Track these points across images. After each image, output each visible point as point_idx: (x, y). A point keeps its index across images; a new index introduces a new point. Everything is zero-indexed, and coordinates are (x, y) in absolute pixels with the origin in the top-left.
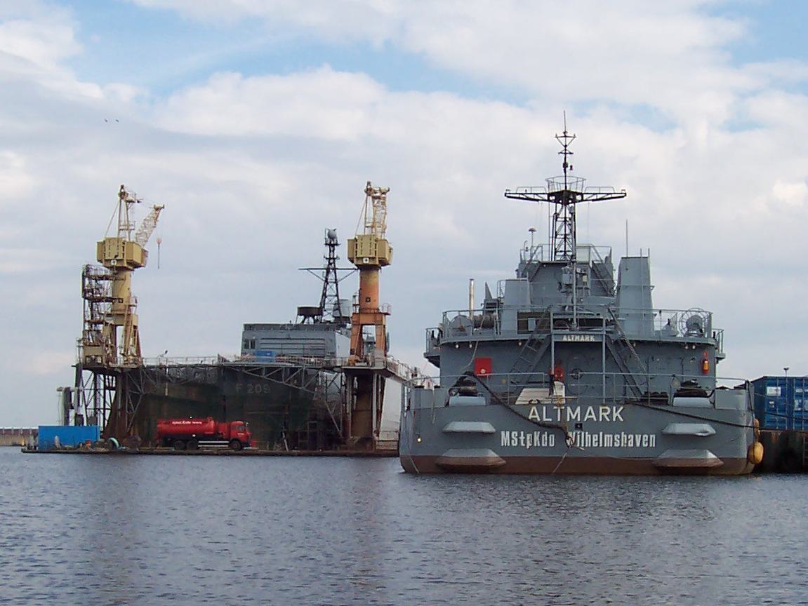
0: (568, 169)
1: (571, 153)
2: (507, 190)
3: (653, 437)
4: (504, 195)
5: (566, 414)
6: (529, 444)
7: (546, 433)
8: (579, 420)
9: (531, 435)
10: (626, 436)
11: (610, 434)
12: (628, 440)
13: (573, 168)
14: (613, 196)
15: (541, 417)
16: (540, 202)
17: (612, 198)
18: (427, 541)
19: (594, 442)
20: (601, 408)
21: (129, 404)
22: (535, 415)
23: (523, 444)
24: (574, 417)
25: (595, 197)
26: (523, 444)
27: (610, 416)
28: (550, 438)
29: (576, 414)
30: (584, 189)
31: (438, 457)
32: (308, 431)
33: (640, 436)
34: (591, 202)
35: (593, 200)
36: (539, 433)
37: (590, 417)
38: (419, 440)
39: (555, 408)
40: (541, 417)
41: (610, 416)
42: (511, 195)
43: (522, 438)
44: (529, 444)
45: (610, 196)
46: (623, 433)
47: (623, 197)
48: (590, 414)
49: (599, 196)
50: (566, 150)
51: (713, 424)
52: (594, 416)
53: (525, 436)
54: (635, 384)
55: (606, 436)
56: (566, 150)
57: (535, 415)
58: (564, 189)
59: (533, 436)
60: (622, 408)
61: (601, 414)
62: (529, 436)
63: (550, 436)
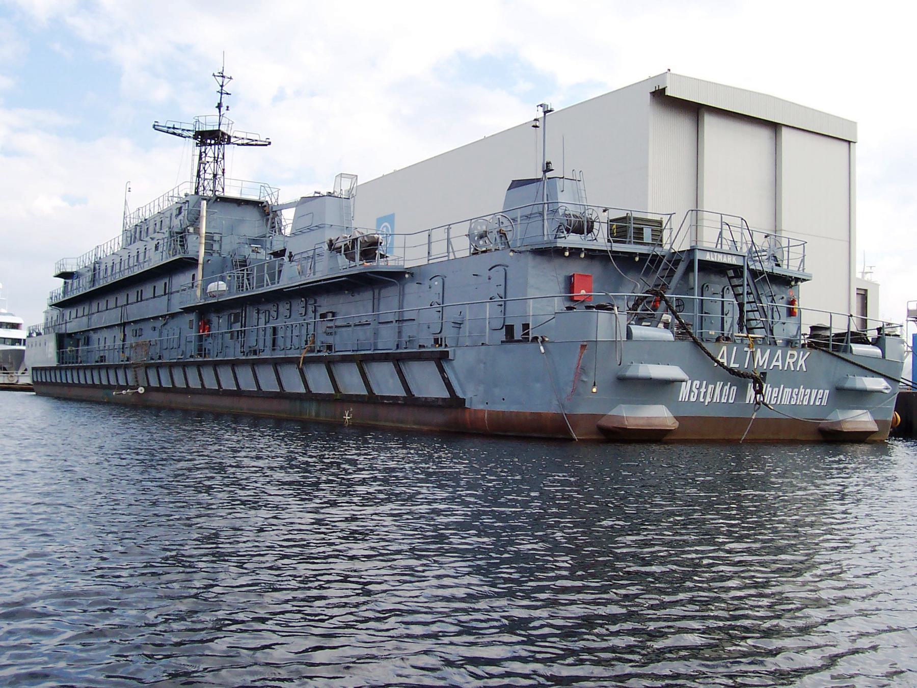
0: (223, 109)
1: (227, 94)
2: (156, 122)
3: (827, 392)
4: (152, 126)
5: (776, 354)
6: (708, 399)
7: (729, 384)
8: (765, 368)
9: (713, 386)
10: (803, 390)
11: (789, 388)
12: (805, 395)
13: (229, 109)
14: (259, 143)
15: (729, 361)
16: (187, 138)
17: (256, 145)
18: (162, 465)
19: (773, 397)
20: (790, 352)
21: (267, 281)
22: (723, 358)
23: (702, 400)
24: (761, 364)
25: (240, 142)
26: (702, 400)
27: (795, 363)
28: (732, 390)
29: (764, 359)
30: (232, 131)
31: (603, 416)
32: (80, 348)
33: (816, 390)
34: (236, 145)
35: (238, 145)
36: (722, 383)
37: (777, 364)
38: (594, 390)
39: (746, 349)
40: (729, 361)
41: (795, 363)
42: (161, 128)
43: (703, 390)
44: (708, 399)
45: (254, 143)
46: (802, 387)
47: (266, 145)
48: (777, 360)
49: (245, 141)
50: (222, 90)
51: (889, 381)
52: (780, 364)
53: (707, 387)
54: (766, 317)
55: (786, 390)
56: (222, 90)
57: (723, 358)
58: (217, 129)
59: (715, 388)
60: (808, 353)
61: (788, 360)
62: (711, 387)
63: (733, 388)
